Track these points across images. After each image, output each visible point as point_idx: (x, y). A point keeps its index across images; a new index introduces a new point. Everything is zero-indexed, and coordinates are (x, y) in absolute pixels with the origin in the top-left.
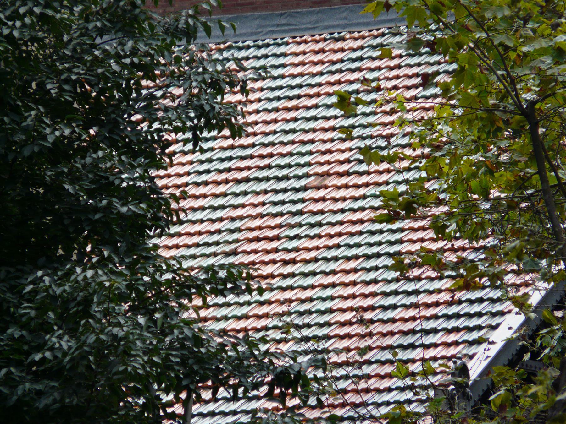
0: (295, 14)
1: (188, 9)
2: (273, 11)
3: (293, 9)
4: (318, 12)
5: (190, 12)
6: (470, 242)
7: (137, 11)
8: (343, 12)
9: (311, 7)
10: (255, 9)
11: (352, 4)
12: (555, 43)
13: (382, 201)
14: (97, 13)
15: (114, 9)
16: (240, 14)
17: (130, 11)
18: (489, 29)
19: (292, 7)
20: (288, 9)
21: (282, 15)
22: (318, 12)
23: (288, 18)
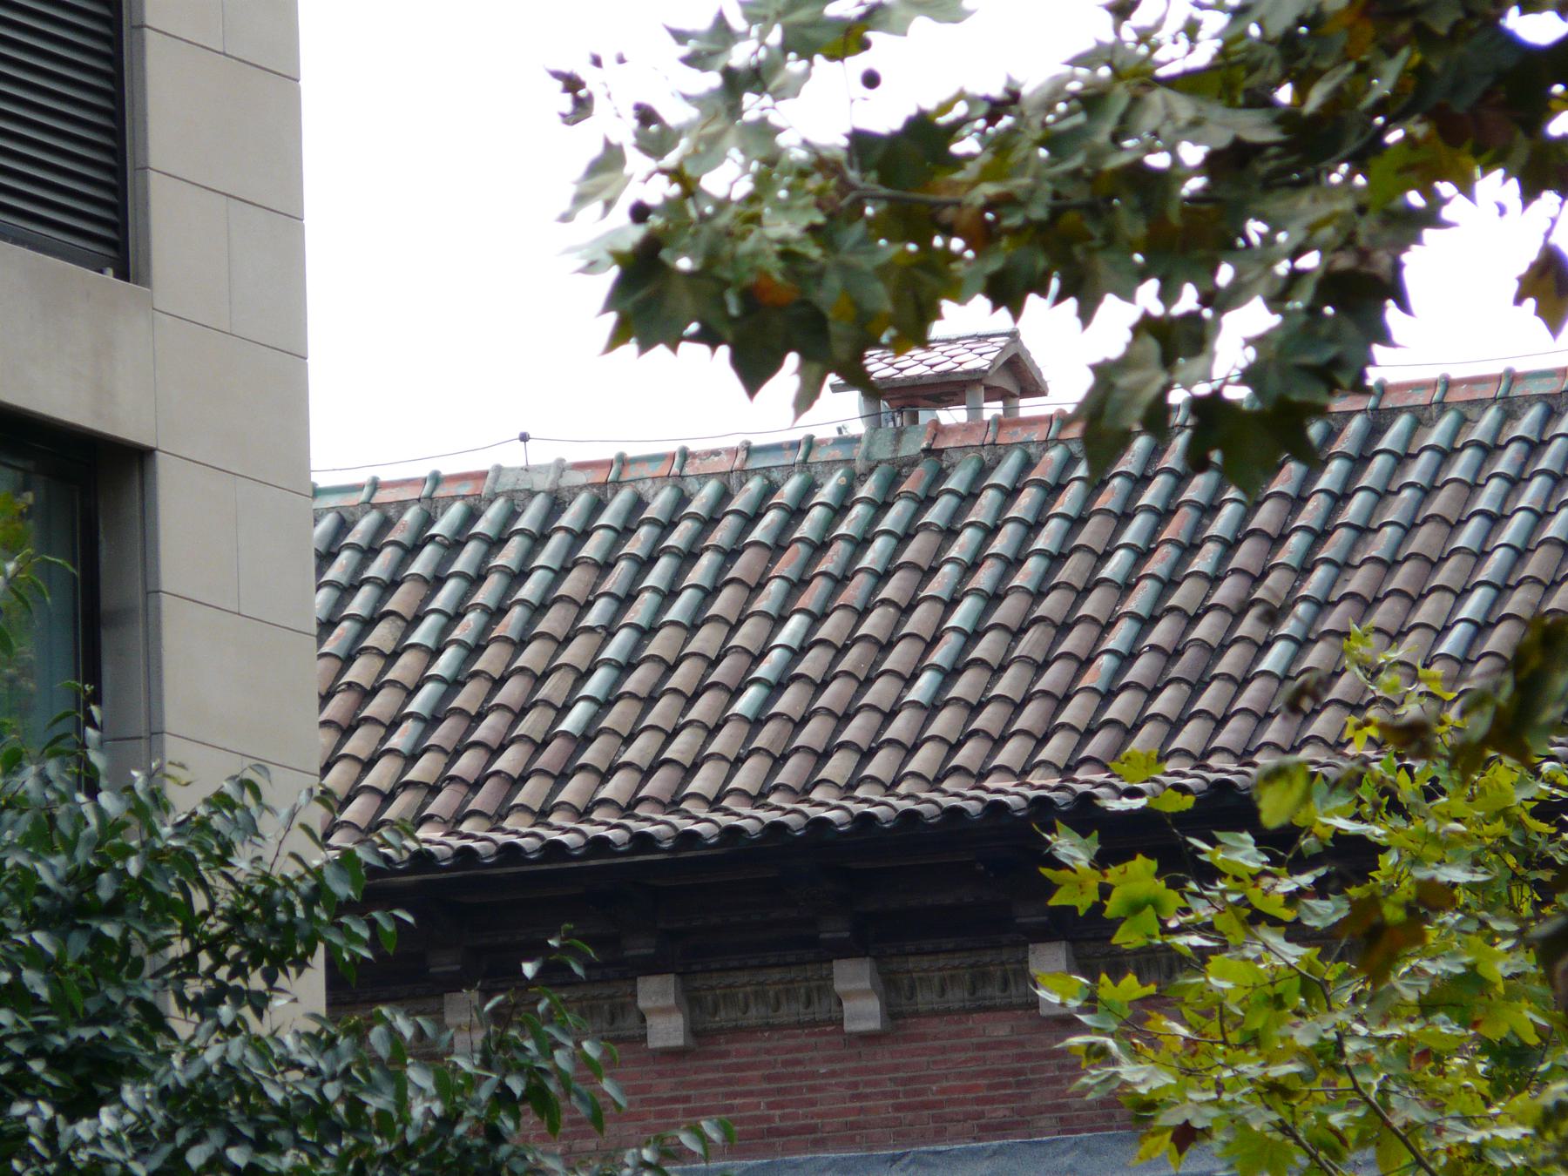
0: (931, 1158)
1: (640, 1147)
2: (870, 1149)
3: (925, 1144)
4: (996, 1153)
5: (647, 1155)
6: (89, 839)
7: (504, 1150)
8: (1065, 1153)
9: (975, 1139)
10: (819, 1144)
11: (1090, 1130)
12: (1198, 918)
13: (236, 804)
14: (387, 1157)
15: (436, 1145)
16: (779, 1159)
17: (484, 1151)
18: (1449, 933)
19: (923, 1138)
20: (912, 1145)
21: (894, 1159)
22: (996, 1153)
23: (912, 1169)
